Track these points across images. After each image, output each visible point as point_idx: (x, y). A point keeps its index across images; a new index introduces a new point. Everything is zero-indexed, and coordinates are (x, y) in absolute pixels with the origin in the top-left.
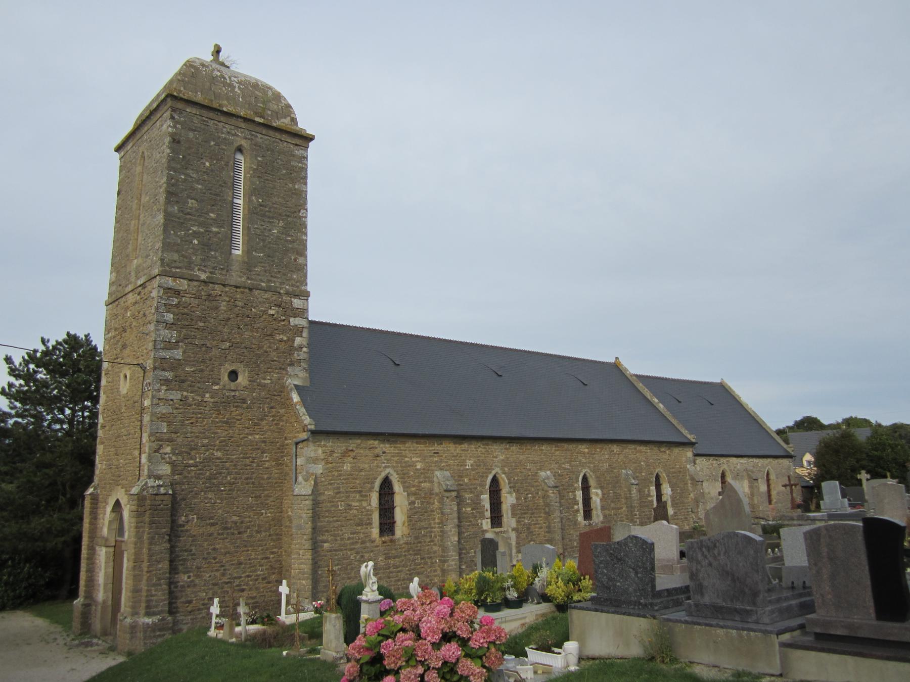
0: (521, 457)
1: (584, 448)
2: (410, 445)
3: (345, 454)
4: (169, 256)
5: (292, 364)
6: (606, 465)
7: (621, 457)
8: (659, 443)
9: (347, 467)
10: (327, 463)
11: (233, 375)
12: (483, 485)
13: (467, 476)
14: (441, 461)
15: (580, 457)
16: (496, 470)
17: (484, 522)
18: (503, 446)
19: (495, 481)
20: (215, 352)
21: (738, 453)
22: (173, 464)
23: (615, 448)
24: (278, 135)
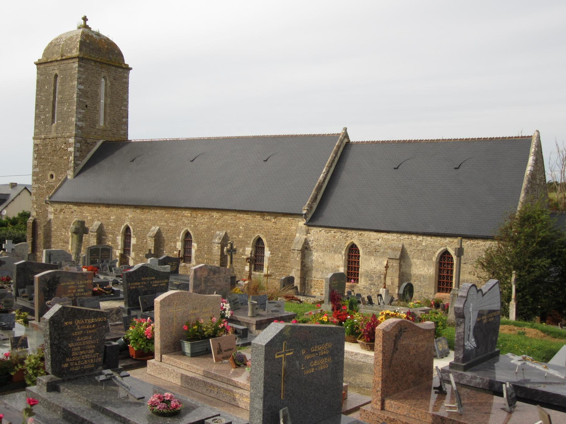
0: (143, 217)
1: (187, 213)
2: (86, 207)
3: (61, 210)
4: (80, 124)
5: (68, 169)
6: (204, 227)
7: (220, 222)
8: (262, 213)
9: (61, 217)
10: (55, 214)
11: (52, 176)
12: (119, 231)
13: (111, 225)
14: (99, 216)
15: (184, 219)
16: (127, 223)
17: (117, 251)
18: (132, 210)
19: (127, 229)
20: (47, 168)
21: (441, 231)
22: (36, 212)
23: (215, 215)
24: (67, 61)
